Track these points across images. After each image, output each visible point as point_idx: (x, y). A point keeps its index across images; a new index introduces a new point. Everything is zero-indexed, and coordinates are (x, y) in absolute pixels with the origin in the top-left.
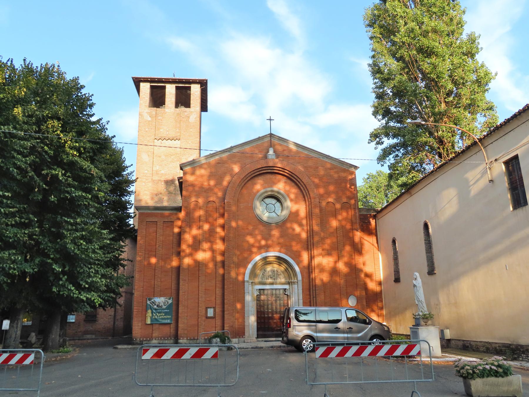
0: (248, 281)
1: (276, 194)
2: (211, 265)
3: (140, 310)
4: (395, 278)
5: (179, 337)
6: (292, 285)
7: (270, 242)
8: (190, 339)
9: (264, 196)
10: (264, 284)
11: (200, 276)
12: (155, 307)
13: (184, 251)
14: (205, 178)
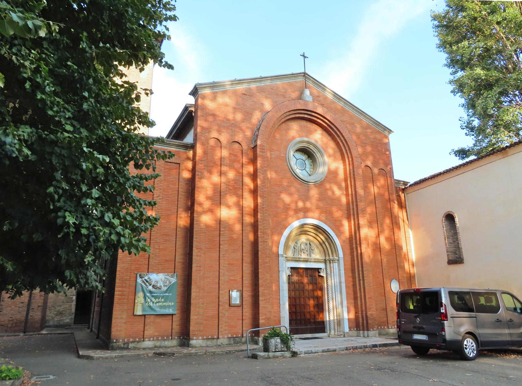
0: (282, 256)
1: (311, 147)
2: (238, 227)
3: (125, 293)
4: (448, 260)
5: (191, 336)
6: (330, 263)
7: (308, 205)
8: (208, 339)
9: (302, 145)
10: (298, 260)
11: (221, 243)
12: (150, 288)
13: (200, 204)
14: (230, 109)
